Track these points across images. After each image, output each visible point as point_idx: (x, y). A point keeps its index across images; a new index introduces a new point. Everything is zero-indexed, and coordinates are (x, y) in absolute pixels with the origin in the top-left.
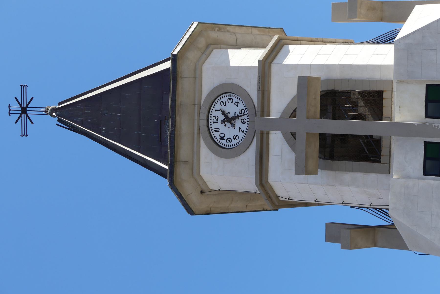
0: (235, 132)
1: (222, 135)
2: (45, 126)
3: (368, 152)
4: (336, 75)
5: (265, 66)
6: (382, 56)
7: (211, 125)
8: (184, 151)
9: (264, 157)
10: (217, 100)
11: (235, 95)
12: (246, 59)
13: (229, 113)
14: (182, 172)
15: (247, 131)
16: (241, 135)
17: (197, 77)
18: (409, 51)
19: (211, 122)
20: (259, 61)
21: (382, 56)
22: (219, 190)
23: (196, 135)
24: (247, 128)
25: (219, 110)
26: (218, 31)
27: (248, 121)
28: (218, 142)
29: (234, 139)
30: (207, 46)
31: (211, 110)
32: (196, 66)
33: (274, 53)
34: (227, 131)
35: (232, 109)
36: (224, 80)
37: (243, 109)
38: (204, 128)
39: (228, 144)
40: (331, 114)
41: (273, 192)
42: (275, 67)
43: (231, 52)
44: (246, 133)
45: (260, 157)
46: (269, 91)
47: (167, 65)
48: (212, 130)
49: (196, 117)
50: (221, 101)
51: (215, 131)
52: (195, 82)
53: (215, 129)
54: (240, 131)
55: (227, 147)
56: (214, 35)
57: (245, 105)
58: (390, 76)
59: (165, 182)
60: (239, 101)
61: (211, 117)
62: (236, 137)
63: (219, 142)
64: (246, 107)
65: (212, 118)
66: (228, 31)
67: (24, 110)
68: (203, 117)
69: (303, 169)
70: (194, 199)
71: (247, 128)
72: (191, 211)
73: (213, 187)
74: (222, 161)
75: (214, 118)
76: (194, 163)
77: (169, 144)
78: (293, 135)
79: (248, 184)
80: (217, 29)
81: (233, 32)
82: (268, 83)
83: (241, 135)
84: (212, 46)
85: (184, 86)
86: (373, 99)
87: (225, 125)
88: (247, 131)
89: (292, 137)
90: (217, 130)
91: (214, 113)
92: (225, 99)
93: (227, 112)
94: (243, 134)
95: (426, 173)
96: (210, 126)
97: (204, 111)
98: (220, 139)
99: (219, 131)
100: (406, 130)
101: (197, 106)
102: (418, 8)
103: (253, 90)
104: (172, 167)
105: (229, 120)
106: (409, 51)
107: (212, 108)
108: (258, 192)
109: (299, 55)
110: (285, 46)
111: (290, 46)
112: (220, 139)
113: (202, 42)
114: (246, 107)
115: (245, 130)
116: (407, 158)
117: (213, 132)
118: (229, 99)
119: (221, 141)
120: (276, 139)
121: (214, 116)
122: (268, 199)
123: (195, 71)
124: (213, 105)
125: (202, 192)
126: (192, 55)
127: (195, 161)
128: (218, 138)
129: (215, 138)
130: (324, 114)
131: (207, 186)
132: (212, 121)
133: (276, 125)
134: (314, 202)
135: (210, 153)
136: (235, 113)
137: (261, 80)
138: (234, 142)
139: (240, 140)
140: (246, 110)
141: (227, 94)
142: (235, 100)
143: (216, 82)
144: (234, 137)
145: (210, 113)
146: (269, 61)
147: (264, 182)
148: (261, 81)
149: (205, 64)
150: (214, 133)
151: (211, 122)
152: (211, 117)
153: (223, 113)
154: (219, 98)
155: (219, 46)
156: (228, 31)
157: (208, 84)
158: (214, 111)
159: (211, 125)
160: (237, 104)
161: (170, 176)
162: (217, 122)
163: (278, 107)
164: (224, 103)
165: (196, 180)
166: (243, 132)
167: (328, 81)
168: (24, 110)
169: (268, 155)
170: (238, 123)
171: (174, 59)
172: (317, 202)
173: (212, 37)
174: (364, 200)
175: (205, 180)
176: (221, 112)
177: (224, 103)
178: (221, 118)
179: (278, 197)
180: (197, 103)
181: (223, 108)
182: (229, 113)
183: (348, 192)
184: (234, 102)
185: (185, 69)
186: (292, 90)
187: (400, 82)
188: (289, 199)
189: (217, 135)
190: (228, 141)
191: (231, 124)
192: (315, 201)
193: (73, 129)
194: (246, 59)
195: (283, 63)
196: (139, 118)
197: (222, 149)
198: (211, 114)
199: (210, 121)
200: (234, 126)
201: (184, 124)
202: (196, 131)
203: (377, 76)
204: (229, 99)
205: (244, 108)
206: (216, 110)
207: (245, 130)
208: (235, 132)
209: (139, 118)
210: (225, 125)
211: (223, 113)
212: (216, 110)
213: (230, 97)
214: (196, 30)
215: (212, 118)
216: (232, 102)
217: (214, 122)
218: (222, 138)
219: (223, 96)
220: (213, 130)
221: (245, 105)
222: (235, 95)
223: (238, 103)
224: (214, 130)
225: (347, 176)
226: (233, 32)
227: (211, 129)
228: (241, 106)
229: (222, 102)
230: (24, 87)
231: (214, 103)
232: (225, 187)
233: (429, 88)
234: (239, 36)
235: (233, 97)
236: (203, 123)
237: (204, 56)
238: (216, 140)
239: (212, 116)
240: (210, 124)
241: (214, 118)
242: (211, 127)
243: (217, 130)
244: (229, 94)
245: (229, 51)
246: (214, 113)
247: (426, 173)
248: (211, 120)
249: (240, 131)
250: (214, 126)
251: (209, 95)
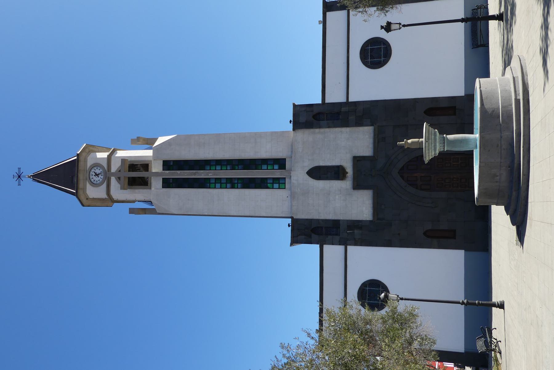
0: (99, 179)
2: (28, 182)
3: (143, 183)
4: (133, 159)
5: (109, 157)
6: (149, 153)
8: (81, 185)
12: (103, 155)
14: (81, 192)
17: (86, 161)
18: (157, 150)
21: (149, 153)
30: (89, 152)
34: (96, 179)
35: (98, 171)
42: (112, 157)
47: (76, 158)
56: (91, 148)
58: (151, 159)
59: (75, 197)
67: (19, 177)
68: (88, 174)
69: (123, 188)
70: (84, 201)
72: (83, 205)
73: (91, 197)
76: (84, 189)
77: (438, 138)
78: (119, 178)
79: (104, 195)
85: (81, 164)
86: (145, 166)
89: (119, 179)
90: (92, 178)
95: (163, 187)
100: (157, 174)
102: (160, 138)
103: (105, 165)
104: (77, 192)
105: (97, 175)
106: (157, 150)
109: (121, 154)
113: (87, 150)
116: (156, 183)
120: (113, 180)
122: (109, 201)
126: (84, 154)
130: (129, 171)
133: (113, 174)
143: (92, 163)
157: (90, 163)
161: (76, 194)
163: (114, 169)
167: (131, 161)
168: (19, 177)
170: (100, 176)
171: (78, 155)
173: (90, 149)
174: (142, 198)
178: (94, 174)
183: (138, 194)
185: (82, 159)
186: (119, 164)
187: (154, 160)
189: (92, 180)
193: (38, 182)
194: (103, 155)
196: (65, 176)
197: (93, 184)
201: (81, 176)
203: (147, 159)
208: (99, 179)
209: (65, 176)
225: (137, 191)
228: (101, 170)
230: (19, 169)
232: (95, 197)
233: (164, 161)
243: (92, 178)
246: (91, 173)
247: (163, 187)
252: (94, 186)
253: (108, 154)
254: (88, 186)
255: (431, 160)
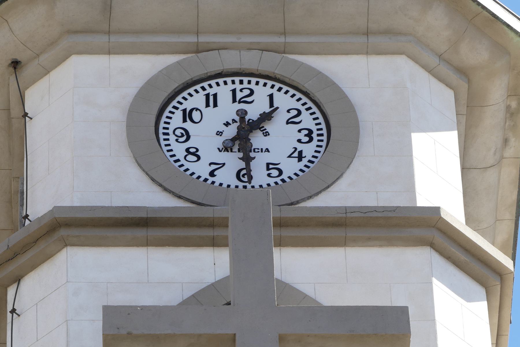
1: (196, 116)
5: (420, 228)
7: (225, 83)
9: (140, 233)
10: (305, 99)
11: (322, 150)
13: (266, 134)
15: (217, 184)
16: (202, 169)
19: (233, 82)
20: (437, 210)
22: (26, 115)
23: (192, 39)
24: (225, 186)
25: (271, 104)
26: (508, 107)
27: (245, 187)
28: (174, 103)
29: (187, 150)
30: (463, 72)
31: (270, 83)
32: (405, 34)
33: (462, 257)
35: (278, 143)
36: (366, 116)
37: (281, 172)
38: (214, 62)
39: (170, 131)
40: (465, 117)
41: (33, 266)
42: (421, 257)
43: (450, 140)
44: (209, 182)
45: (141, 219)
46: (343, 243)
48: (210, 86)
49: (247, 39)
50: (303, 109)
51: (207, 96)
52: (356, 33)
53: (215, 96)
54: (214, 167)
55: (161, 131)
57: (294, 177)
60: (305, 161)
61: (249, 82)
62: (193, 154)
63: (176, 108)
64: (288, 180)
65: (245, 85)
66: (506, 141)
68: (249, 60)
71: (225, 186)
73: (33, 98)
74: (118, 115)
75: (247, 92)
80: (514, 104)
81: (502, 157)
82: (369, 239)
83: (202, 169)
84: (464, 86)
87: (227, 124)
88: (217, 184)
90: (212, 101)
91: (262, 93)
92: (307, 121)
93: (269, 126)
94: (205, 174)
96: (221, 81)
97: (268, 63)
98: (184, 111)
99: (208, 105)
101: (282, 39)
103: (344, 194)
105: (244, 136)
107: (278, 85)
108: (27, 222)
110: (482, 291)
111: (484, 304)
112: (184, 111)
113: (475, 53)
114: (288, 180)
115: (217, 180)
117: (203, 89)
118: (310, 132)
119: (179, 114)
121: (252, 92)
123: (388, 32)
124: (285, 88)
125: (15, 64)
127: (113, 38)
128: (188, 105)
129: (185, 94)
131: (34, 81)
132: (238, 86)
133: (252, 267)
134: (10, 308)
135: (140, 83)
136: (267, 150)
137: (380, 215)
138: (179, 150)
139: (187, 165)
140: (278, 180)
141: (323, 126)
142: (309, 150)
143: (356, 94)
144: (192, 150)
145: (262, 81)
146: (439, 239)
147: (63, 232)
148: (375, 214)
149: (411, 63)
150: (202, 93)
151: (233, 82)
152: (249, 82)
153: (266, 117)
154: (310, 104)
155: (464, 110)
156: (506, 141)
158: (268, 90)
159: (225, 83)
160: (296, 154)
162: (234, 101)
164: (296, 120)
165: (52, 44)
166: (212, 174)
169: (147, 243)
170: (233, 161)
172: (9, 315)
175: (55, 74)
176: (268, 110)
177: (296, 120)
178: (253, 113)
179: (18, 280)
180: (290, 39)
181: (281, 117)
182: (266, 134)
184: (300, 147)
188: (13, 311)
189: (196, 100)
190: (178, 132)
191: (233, 140)
192: (13, 311)
194: (435, 173)
195: (435, 281)
197: (154, 116)
198: (257, 83)
199: (237, 79)
200: (227, 148)
202: (203, 39)
204: (310, 132)
205: (284, 176)
206: (271, 96)
207: (217, 180)
210: (227, 124)
211: (266, 117)
212: (271, 96)
213: (314, 135)
214: (512, 34)
215: (245, 85)
216: (299, 141)
217: (234, 91)
218: (187, 115)
219: (318, 114)
220: (209, 90)
221: (294, 177)
222: (322, 150)
223: (300, 157)
224: (212, 91)
226: (502, 157)
227: (213, 82)
228: (290, 167)
229: (299, 113)
231: (292, 91)
232: (35, 132)
234: (491, 176)
235: (315, 142)
236: (231, 60)
237: (433, 61)
238: (179, 98)
239: (253, 86)
240: (229, 80)
241: (247, 92)
242: (218, 84)
243: (212, 101)
244: (324, 132)
245: (456, 133)
246: (262, 93)
248: (241, 82)
249: (214, 167)
250: (224, 92)
251: (318, 75)
252: (133, 141)
253: (454, 213)
254: (137, 70)
255: (431, 283)
